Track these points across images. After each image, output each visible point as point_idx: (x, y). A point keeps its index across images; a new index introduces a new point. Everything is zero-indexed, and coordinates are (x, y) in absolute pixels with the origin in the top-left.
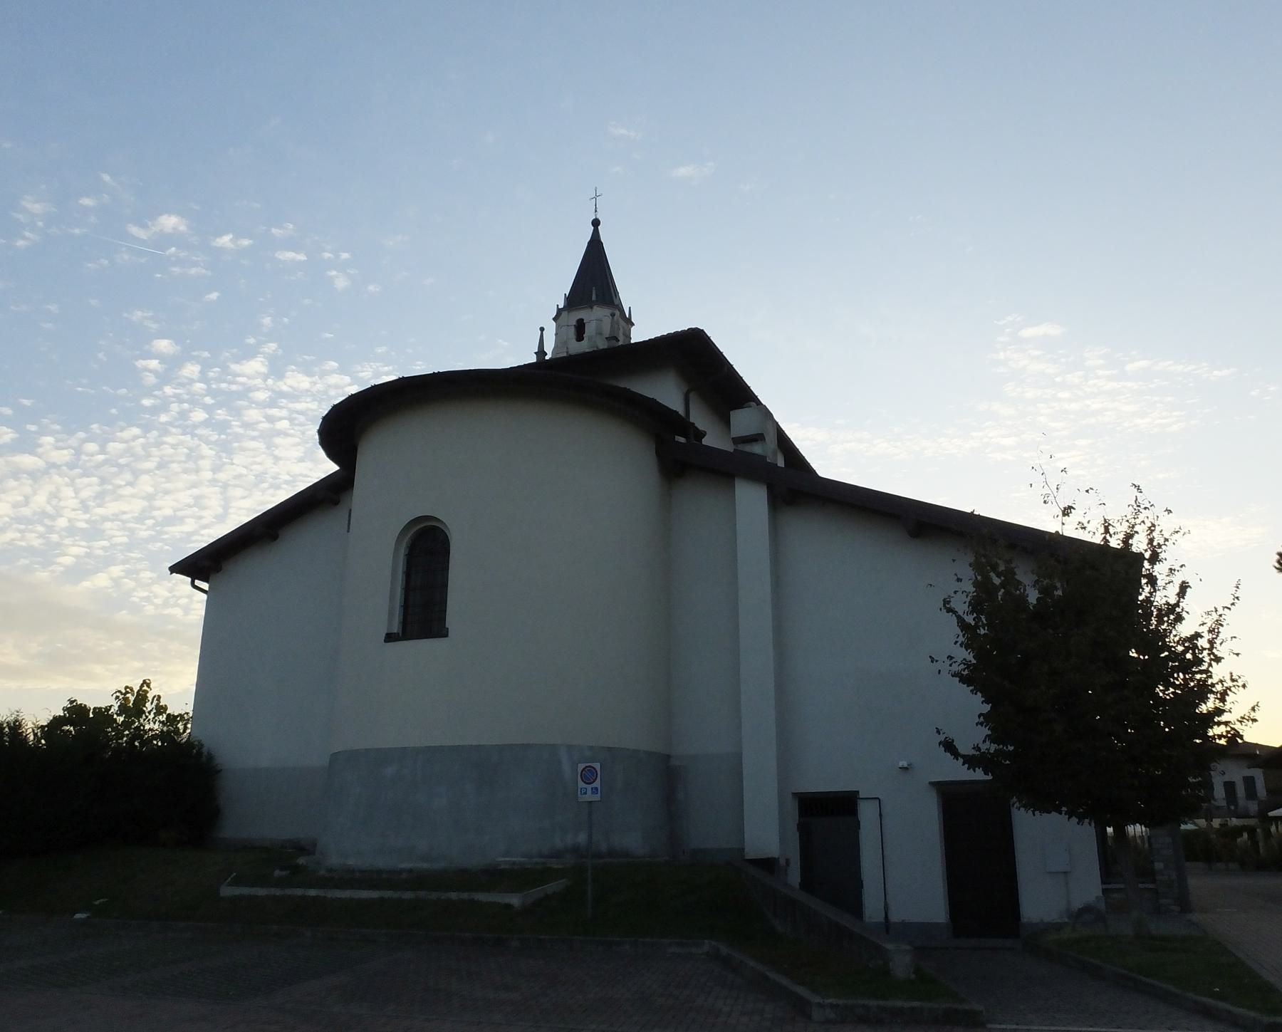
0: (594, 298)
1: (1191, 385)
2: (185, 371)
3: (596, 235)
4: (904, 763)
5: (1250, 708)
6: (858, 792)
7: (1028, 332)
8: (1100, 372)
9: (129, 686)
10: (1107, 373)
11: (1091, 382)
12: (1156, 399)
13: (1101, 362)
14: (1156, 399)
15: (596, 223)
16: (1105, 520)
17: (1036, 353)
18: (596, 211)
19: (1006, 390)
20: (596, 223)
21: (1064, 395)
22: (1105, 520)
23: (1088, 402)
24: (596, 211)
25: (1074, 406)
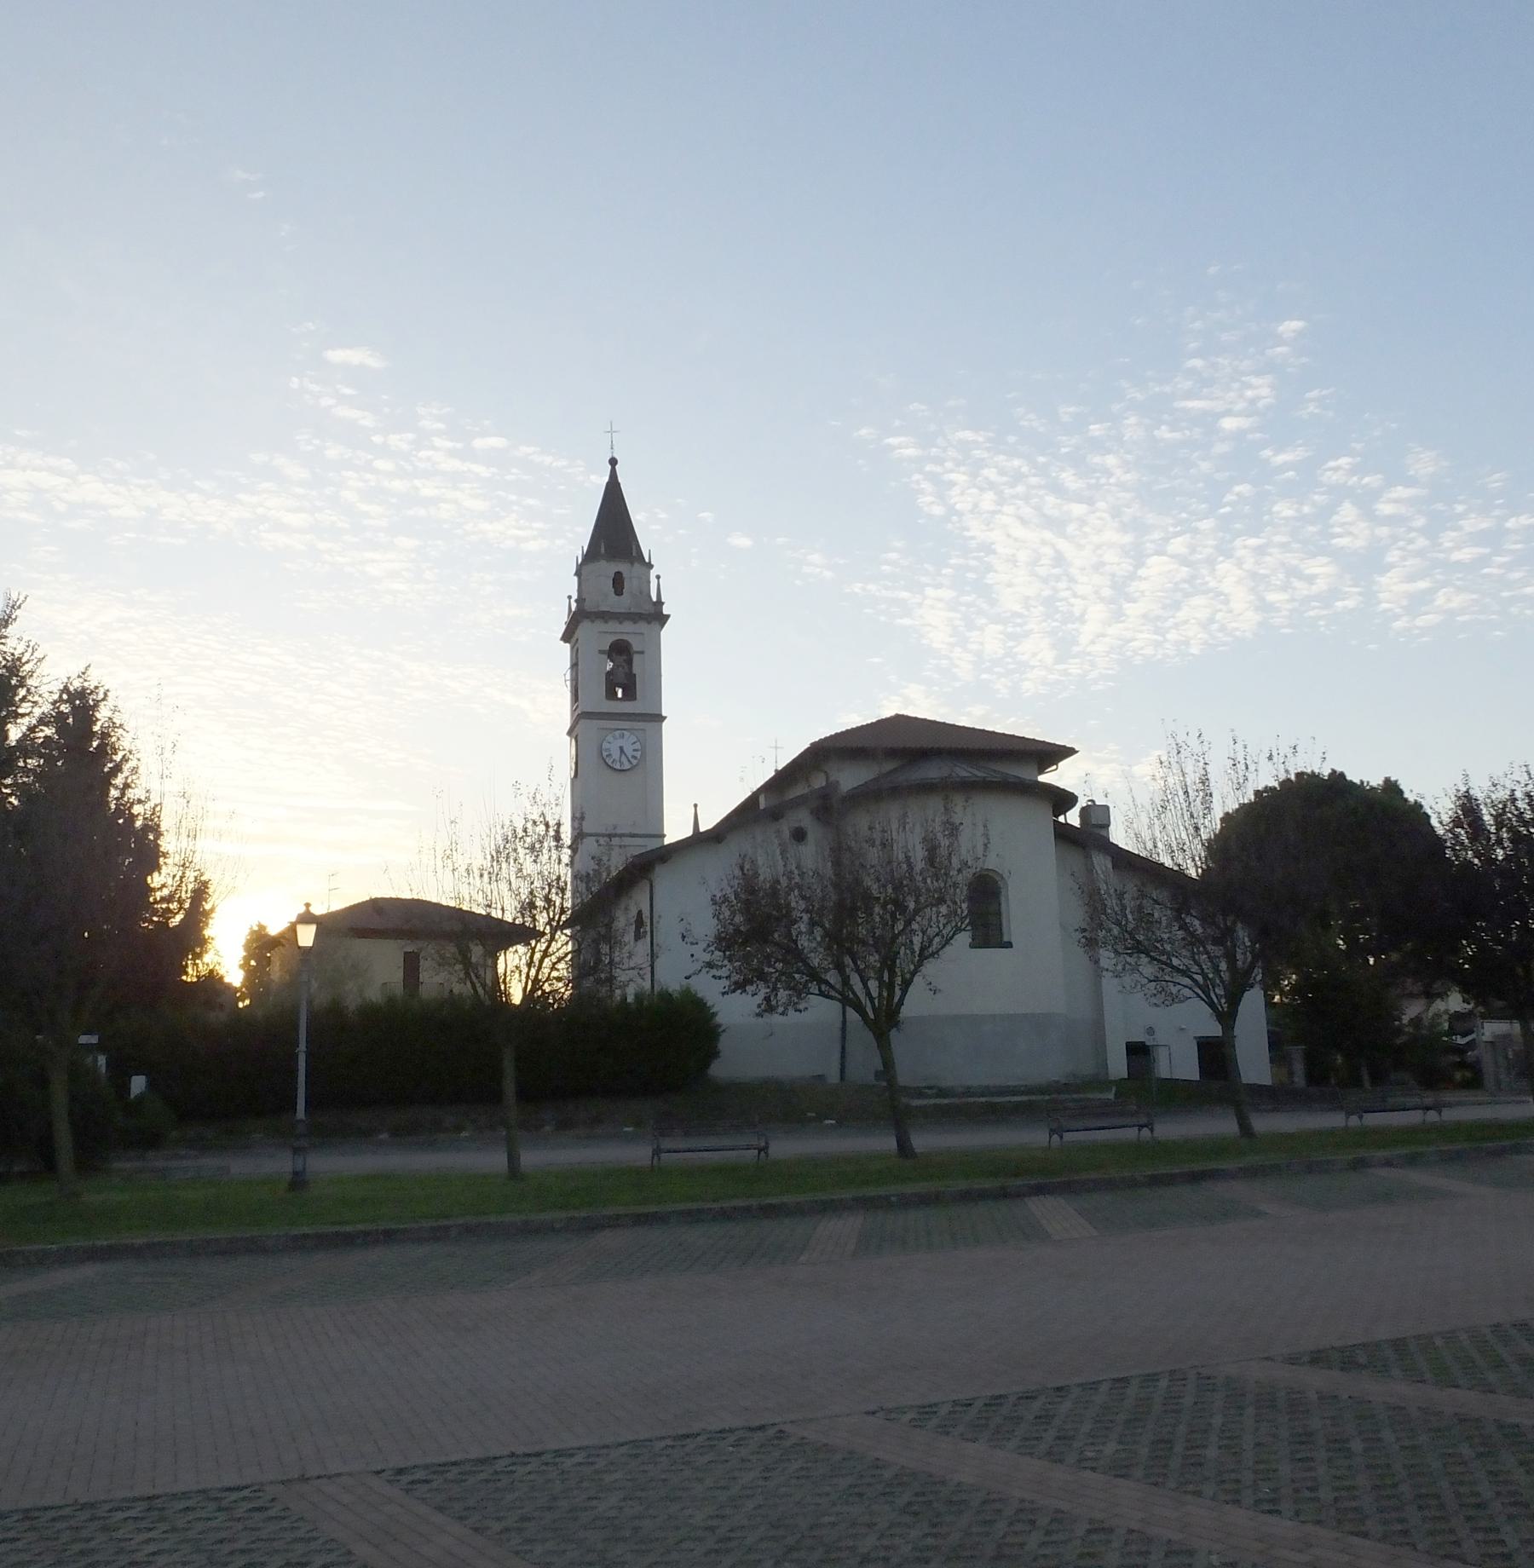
0: (603, 550)
1: (562, 487)
2: (1102, 857)
3: (613, 475)
4: (1183, 1027)
5: (1012, 941)
6: (262, 928)
7: (336, 356)
8: (438, 442)
9: (293, 919)
10: (449, 444)
11: (423, 454)
12: (513, 498)
13: (440, 426)
14: (513, 498)
15: (613, 462)
16: (965, 809)
17: (348, 391)
18: (612, 448)
19: (298, 438)
20: (613, 462)
21: (381, 464)
22: (965, 809)
23: (417, 482)
24: (612, 448)
25: (397, 485)
